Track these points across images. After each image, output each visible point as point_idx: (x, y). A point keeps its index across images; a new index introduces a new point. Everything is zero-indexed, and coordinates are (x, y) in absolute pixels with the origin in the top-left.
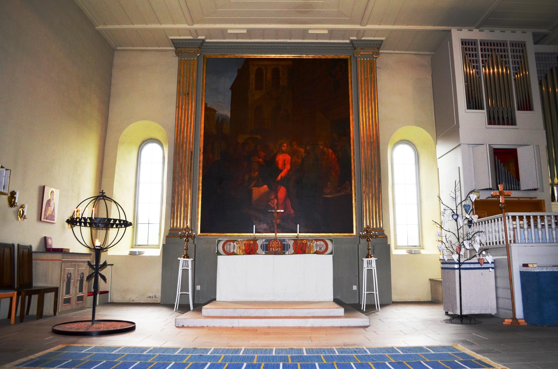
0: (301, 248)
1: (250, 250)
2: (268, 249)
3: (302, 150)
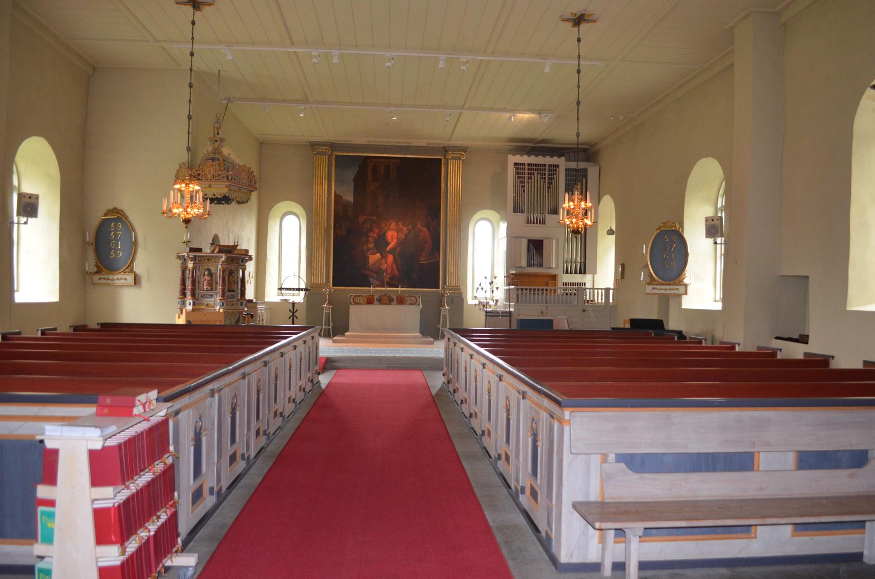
0: (401, 301)
1: (370, 301)
2: (380, 301)
3: (405, 229)
